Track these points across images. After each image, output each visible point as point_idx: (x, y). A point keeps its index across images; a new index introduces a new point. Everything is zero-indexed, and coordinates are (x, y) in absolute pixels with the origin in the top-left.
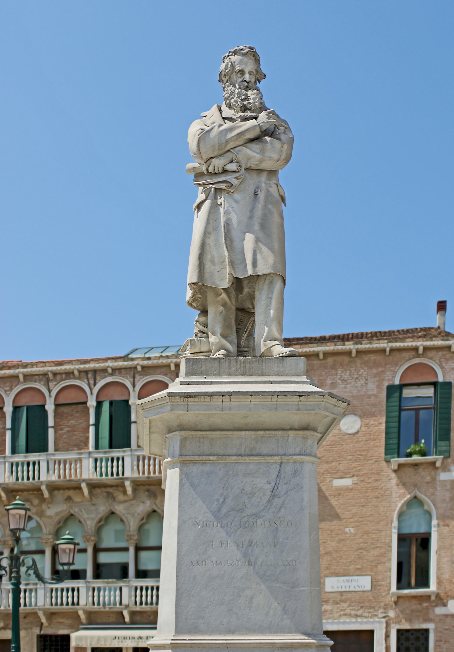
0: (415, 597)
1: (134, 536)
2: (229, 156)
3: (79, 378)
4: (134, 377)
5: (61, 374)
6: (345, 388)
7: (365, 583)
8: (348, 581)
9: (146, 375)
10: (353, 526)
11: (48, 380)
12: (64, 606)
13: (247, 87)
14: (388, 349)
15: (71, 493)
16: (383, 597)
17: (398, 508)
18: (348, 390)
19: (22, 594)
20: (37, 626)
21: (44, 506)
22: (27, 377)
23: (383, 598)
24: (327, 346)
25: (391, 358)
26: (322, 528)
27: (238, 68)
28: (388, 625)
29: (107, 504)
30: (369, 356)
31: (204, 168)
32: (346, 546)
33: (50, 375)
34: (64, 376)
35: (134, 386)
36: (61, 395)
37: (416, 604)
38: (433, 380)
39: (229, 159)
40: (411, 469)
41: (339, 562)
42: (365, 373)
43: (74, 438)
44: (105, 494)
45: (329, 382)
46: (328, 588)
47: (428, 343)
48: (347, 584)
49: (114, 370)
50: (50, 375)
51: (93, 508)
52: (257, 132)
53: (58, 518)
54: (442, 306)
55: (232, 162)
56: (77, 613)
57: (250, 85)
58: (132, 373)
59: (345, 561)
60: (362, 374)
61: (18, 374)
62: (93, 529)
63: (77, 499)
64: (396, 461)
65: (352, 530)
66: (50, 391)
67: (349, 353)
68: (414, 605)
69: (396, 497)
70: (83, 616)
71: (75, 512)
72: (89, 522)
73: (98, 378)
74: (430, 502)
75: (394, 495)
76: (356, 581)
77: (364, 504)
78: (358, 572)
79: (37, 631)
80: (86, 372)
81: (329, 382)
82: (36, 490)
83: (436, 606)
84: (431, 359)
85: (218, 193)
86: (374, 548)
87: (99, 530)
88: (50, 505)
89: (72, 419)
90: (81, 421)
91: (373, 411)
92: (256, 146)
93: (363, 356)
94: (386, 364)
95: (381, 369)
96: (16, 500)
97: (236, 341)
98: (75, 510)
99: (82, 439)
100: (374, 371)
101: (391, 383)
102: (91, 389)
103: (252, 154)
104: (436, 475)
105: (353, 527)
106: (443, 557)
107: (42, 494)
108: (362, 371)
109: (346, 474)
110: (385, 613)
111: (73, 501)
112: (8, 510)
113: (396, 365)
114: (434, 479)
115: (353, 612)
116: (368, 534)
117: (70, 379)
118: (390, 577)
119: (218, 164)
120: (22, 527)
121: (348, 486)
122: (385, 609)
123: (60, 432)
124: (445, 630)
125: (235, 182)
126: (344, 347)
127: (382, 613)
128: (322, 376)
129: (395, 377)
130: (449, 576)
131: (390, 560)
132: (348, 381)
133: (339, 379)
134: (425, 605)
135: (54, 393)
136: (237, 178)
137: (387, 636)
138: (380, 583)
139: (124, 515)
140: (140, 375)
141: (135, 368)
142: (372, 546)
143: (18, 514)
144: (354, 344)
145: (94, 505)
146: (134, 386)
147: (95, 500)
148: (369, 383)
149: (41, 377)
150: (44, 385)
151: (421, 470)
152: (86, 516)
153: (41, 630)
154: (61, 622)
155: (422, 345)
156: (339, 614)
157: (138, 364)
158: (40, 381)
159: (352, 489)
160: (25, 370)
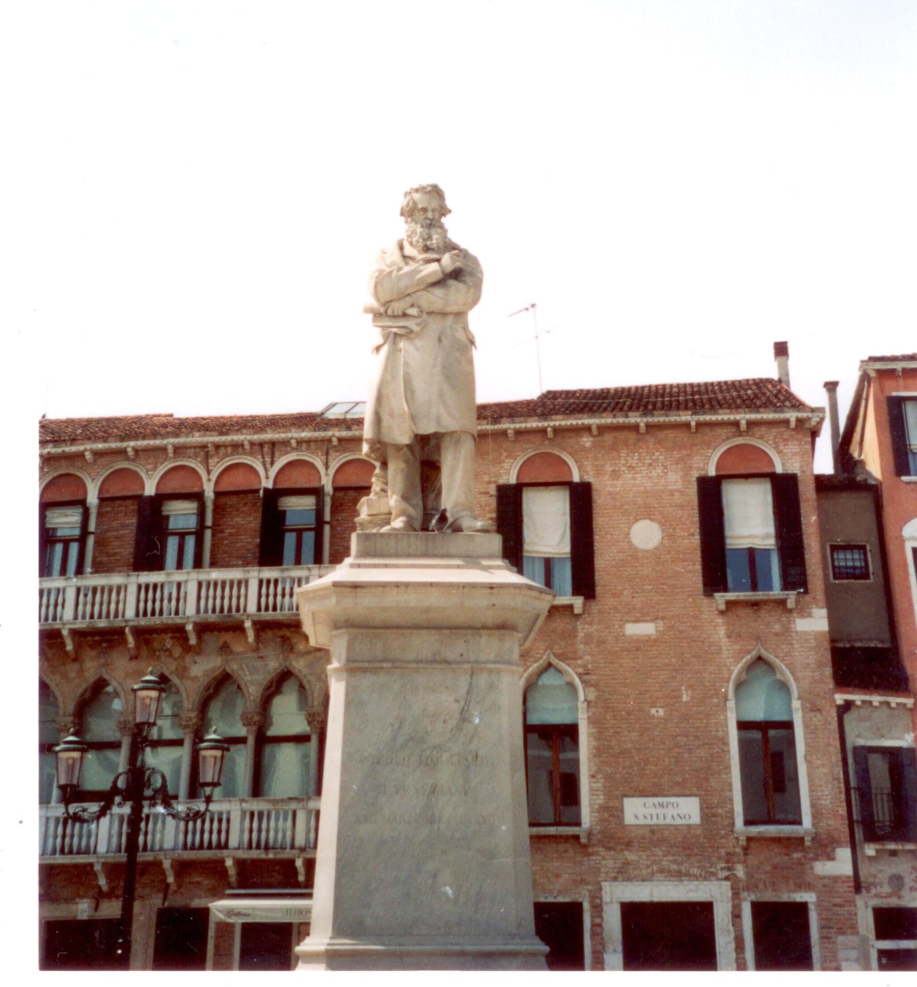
0: (777, 840)
1: (318, 714)
2: (409, 300)
3: (251, 454)
4: (327, 454)
5: (225, 446)
6: (635, 479)
7: (686, 810)
8: (661, 805)
9: (344, 451)
10: (663, 705)
11: (207, 456)
12: (270, 612)
13: (431, 224)
14: (693, 424)
15: (227, 637)
16: (723, 837)
17: (733, 677)
18: (638, 482)
19: (143, 825)
20: (159, 891)
21: (188, 659)
22: (179, 450)
23: (724, 841)
24: (602, 417)
25: (699, 436)
26: (613, 707)
27: (420, 206)
28: (736, 894)
29: (281, 656)
30: (666, 432)
31: (382, 310)
32: (653, 739)
33: (211, 448)
34: (229, 450)
35: (327, 468)
36: (225, 477)
37: (780, 854)
38: (767, 470)
39: (409, 304)
40: (748, 611)
41: (644, 769)
42: (661, 457)
43: (239, 545)
44: (279, 640)
45: (609, 468)
46: (629, 819)
47: (754, 416)
48: (661, 811)
49: (300, 442)
50: (211, 448)
51: (260, 663)
52: (439, 276)
53: (207, 680)
54: (781, 350)
55: (412, 306)
56: (222, 862)
57: (434, 222)
58: (325, 448)
59: (654, 768)
60: (658, 459)
61: (166, 445)
62: (258, 700)
63: (238, 648)
64: (721, 598)
65: (661, 712)
66: (209, 472)
67: (636, 427)
68: (777, 857)
69: (728, 658)
70: (232, 872)
71: (233, 671)
72: (252, 689)
73: (277, 454)
74: (784, 667)
75: (725, 654)
76: (675, 805)
77: (677, 667)
78: (677, 790)
79: (157, 901)
80: (261, 445)
81: (609, 468)
82: (178, 631)
83: (816, 859)
84: (761, 438)
85: (398, 339)
86: (699, 747)
87: (266, 702)
88: (197, 659)
89: (237, 516)
90: (251, 519)
91: (679, 515)
92: (438, 292)
93: (657, 432)
94: (692, 446)
95: (685, 452)
96: (146, 675)
97: (420, 503)
98: (233, 667)
99: (250, 546)
100: (676, 454)
101: (703, 473)
102: (266, 470)
103: (435, 298)
104: (789, 622)
105: (662, 707)
106: (818, 768)
107: (186, 639)
108: (657, 454)
109: (644, 615)
110: (729, 869)
111: (231, 652)
112: (134, 691)
113: (709, 446)
114: (787, 630)
115: (674, 867)
116: (687, 720)
117: (237, 454)
118: (731, 800)
119: (397, 307)
120: (152, 720)
121: (649, 636)
122: (727, 862)
123: (219, 535)
124: (835, 905)
125: (416, 329)
126: (627, 420)
127: (722, 869)
128: (597, 460)
129: (708, 464)
130: (831, 803)
131: (728, 768)
132: (637, 469)
133: (624, 465)
134: (796, 855)
135: (214, 476)
136: (418, 324)
137: (736, 916)
138: (714, 810)
139: (305, 676)
140: (336, 451)
141: (330, 440)
142: (696, 743)
143: (147, 697)
144: (641, 416)
145: (262, 657)
146: (327, 468)
147: (263, 652)
148: (670, 473)
149: (198, 450)
150: (200, 462)
151: (763, 613)
152: (249, 678)
153: (165, 899)
154: (198, 883)
155: (744, 418)
156: (649, 870)
157: (334, 435)
158: (196, 456)
159: (656, 641)
160: (176, 440)
